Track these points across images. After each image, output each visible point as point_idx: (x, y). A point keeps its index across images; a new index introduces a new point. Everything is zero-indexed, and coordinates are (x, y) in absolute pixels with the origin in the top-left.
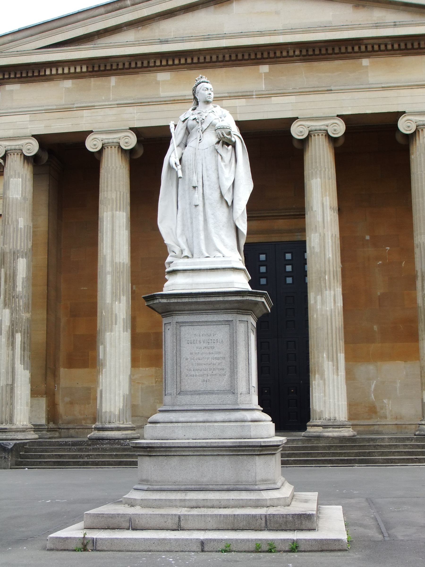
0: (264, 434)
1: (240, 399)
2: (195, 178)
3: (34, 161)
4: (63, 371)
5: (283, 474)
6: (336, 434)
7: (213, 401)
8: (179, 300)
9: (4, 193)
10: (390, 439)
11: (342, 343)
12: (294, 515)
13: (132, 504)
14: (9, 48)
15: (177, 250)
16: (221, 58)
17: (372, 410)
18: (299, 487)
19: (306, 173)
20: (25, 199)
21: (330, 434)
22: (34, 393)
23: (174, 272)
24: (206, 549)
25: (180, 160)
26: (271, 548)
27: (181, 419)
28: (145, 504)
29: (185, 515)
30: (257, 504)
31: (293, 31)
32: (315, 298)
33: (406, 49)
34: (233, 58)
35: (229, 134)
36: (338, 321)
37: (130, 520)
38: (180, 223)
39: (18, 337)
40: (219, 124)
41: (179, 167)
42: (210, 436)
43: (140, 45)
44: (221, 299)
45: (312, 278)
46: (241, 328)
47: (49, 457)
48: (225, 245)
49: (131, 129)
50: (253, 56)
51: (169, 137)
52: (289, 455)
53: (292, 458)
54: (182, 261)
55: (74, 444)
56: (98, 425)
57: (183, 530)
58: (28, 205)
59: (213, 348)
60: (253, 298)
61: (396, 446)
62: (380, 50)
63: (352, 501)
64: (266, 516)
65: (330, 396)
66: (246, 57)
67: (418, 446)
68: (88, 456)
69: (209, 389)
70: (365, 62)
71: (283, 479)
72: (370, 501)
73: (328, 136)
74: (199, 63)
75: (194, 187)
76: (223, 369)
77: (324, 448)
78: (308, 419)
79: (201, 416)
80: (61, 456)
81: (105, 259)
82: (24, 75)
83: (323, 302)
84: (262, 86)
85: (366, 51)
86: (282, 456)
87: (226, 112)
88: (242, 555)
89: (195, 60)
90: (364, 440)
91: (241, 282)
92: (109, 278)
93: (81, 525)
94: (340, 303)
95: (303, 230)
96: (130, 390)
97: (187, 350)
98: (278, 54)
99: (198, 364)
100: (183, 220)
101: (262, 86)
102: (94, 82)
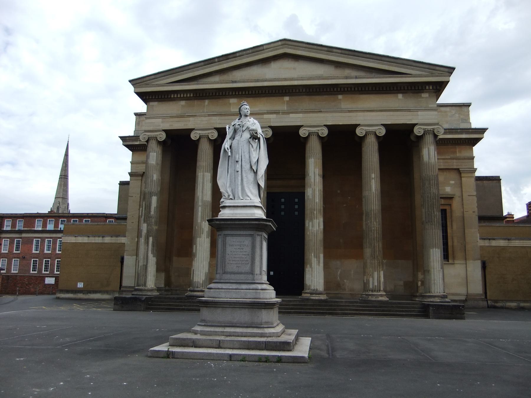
0: (268, 296)
1: (256, 277)
2: (237, 156)
3: (162, 144)
4: (175, 259)
5: (279, 319)
6: (317, 298)
7: (242, 278)
8: (226, 223)
9: (147, 161)
10: (346, 302)
11: (322, 249)
12: (280, 342)
13: (196, 333)
14: (152, 82)
15: (226, 195)
16: (264, 92)
17: (339, 286)
18: (288, 326)
19: (306, 155)
20: (157, 164)
21: (314, 298)
22: (158, 270)
23: (224, 207)
24: (232, 359)
25: (231, 147)
26: (267, 360)
27: (224, 287)
28: (203, 333)
29: (223, 340)
30: (262, 335)
31: (302, 79)
32: (309, 223)
33: (362, 90)
34: (270, 92)
35: (256, 133)
36: (320, 236)
37: (194, 342)
38: (229, 180)
39: (151, 239)
40: (252, 127)
41: (230, 150)
42: (239, 297)
43: (221, 83)
44: (248, 222)
45: (307, 212)
46: (258, 239)
47: (164, 305)
48: (252, 193)
49: (215, 128)
50: (281, 92)
51: (225, 134)
52: (282, 309)
53: (284, 310)
54: (228, 201)
55: (178, 299)
56: (191, 288)
57: (221, 348)
58: (159, 167)
59: (242, 249)
60: (265, 223)
61: (349, 306)
62: (348, 91)
63: (319, 335)
64: (265, 342)
65: (315, 277)
66: (277, 92)
67: (361, 306)
68: (185, 306)
69: (240, 271)
70: (340, 97)
71: (279, 322)
72: (328, 336)
73: (318, 136)
74: (252, 94)
75: (237, 162)
76: (247, 261)
77: (310, 305)
78: (303, 290)
79: (234, 286)
80: (170, 305)
81: (198, 198)
82: (160, 97)
83: (313, 226)
84: (285, 108)
85: (341, 91)
86: (279, 308)
87: (256, 121)
88: (251, 363)
89: (250, 93)
90: (332, 302)
91: (260, 214)
92: (200, 209)
93: (168, 344)
94: (322, 227)
95: (303, 186)
96: (209, 270)
97: (229, 249)
98: (294, 91)
99: (234, 258)
100: (230, 179)
101: (285, 108)
102: (196, 102)
